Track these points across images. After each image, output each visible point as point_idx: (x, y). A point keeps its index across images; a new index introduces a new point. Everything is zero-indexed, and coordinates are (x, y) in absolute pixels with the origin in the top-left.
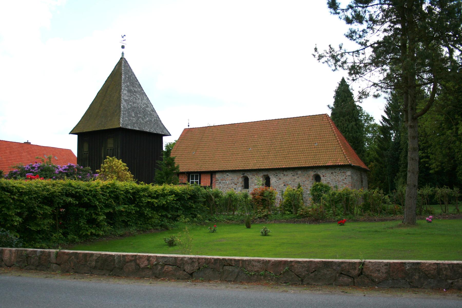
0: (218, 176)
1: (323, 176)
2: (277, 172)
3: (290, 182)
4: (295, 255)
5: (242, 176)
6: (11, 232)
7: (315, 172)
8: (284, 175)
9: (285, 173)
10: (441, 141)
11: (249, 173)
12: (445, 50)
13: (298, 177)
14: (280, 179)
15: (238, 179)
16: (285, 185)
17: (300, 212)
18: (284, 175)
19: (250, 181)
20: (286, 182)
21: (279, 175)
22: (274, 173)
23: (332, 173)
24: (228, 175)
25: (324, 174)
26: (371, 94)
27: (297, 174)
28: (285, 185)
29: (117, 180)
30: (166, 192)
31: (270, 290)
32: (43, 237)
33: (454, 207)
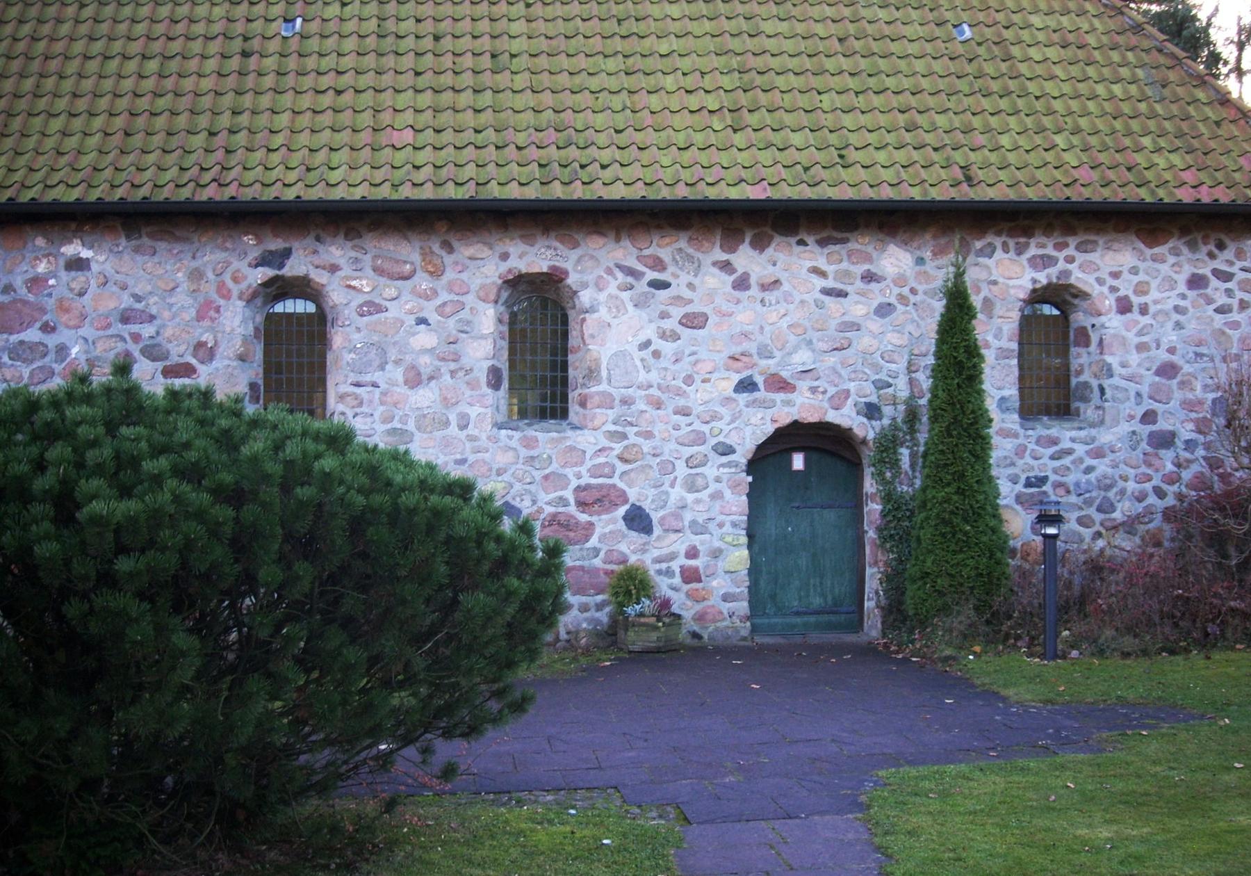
0: (1213, 20)
1: (1124, 307)
2: (667, 247)
3: (803, 358)
4: (549, 212)
5: (261, 275)
6: (597, 622)
7: (1044, 262)
8: (742, 284)
9: (746, 258)
10: (512, 839)
11: (337, 252)
12: (977, 649)
13: (884, 310)
14: (694, 321)
15: (207, 311)
16: (747, 386)
17: (506, 711)
18: (742, 284)
19: (346, 341)
20: (765, 353)
21: (680, 281)
22: (624, 252)
23: (1196, 282)
24: (77, 265)
25: (1126, 289)
26: (1125, 269)
27: (869, 277)
28: (747, 386)
29: (123, 368)
30: (190, 510)
31: (611, 245)
32: (1110, 606)
33: (545, 649)
